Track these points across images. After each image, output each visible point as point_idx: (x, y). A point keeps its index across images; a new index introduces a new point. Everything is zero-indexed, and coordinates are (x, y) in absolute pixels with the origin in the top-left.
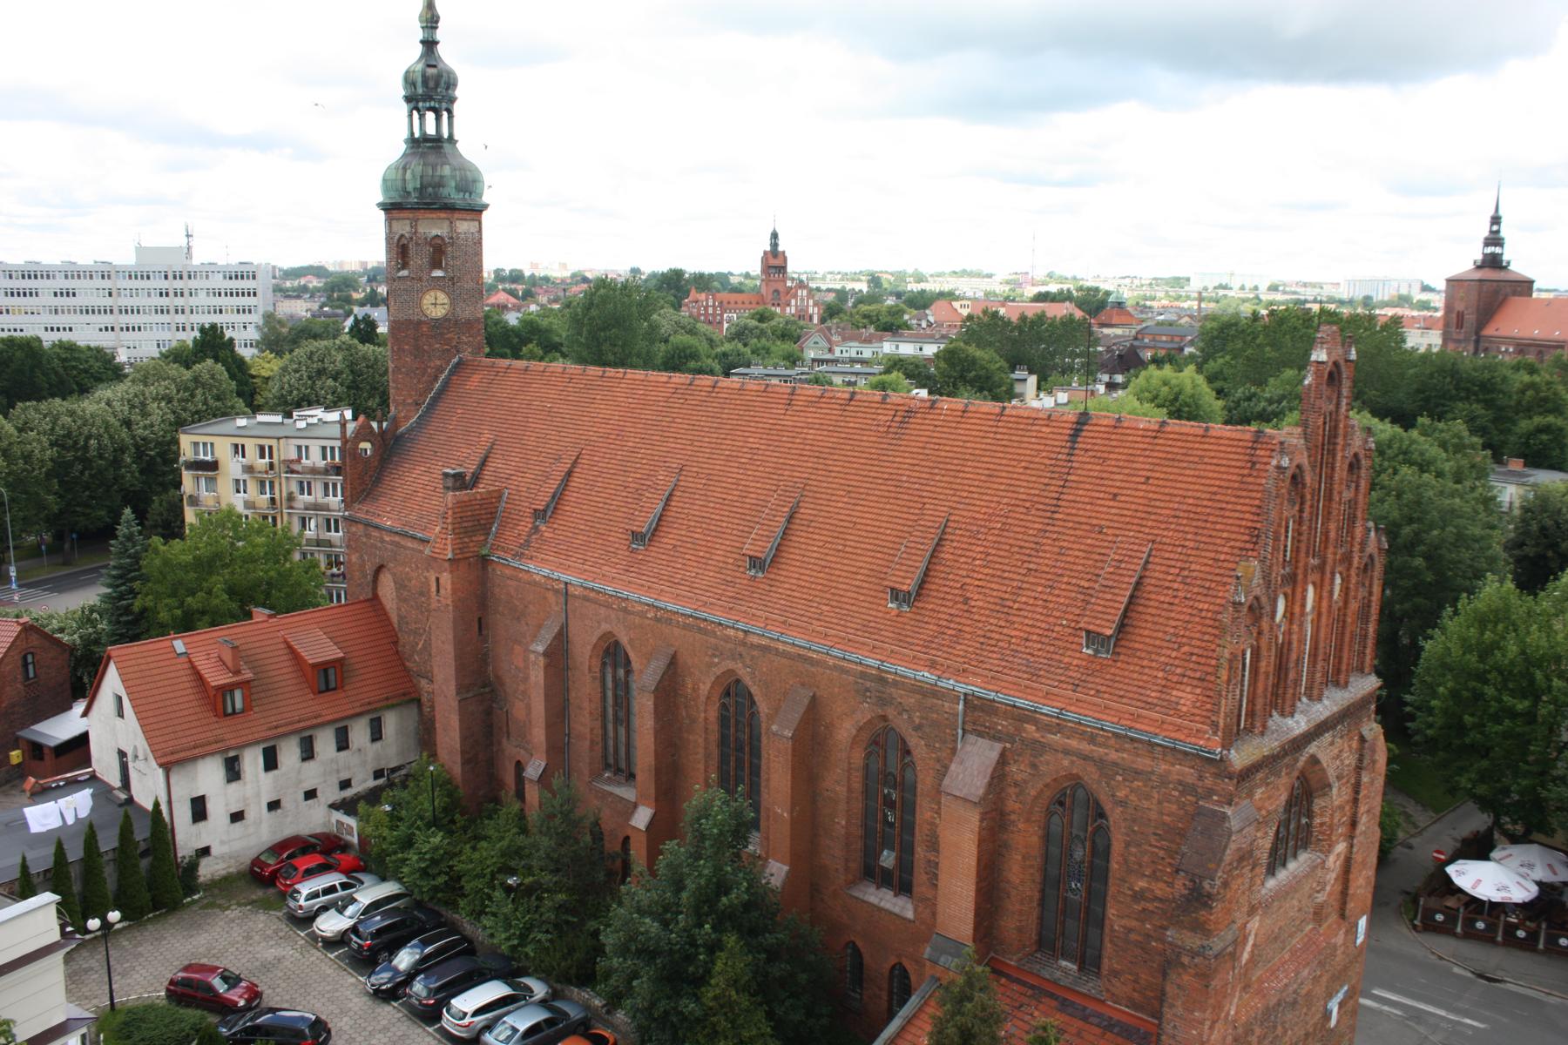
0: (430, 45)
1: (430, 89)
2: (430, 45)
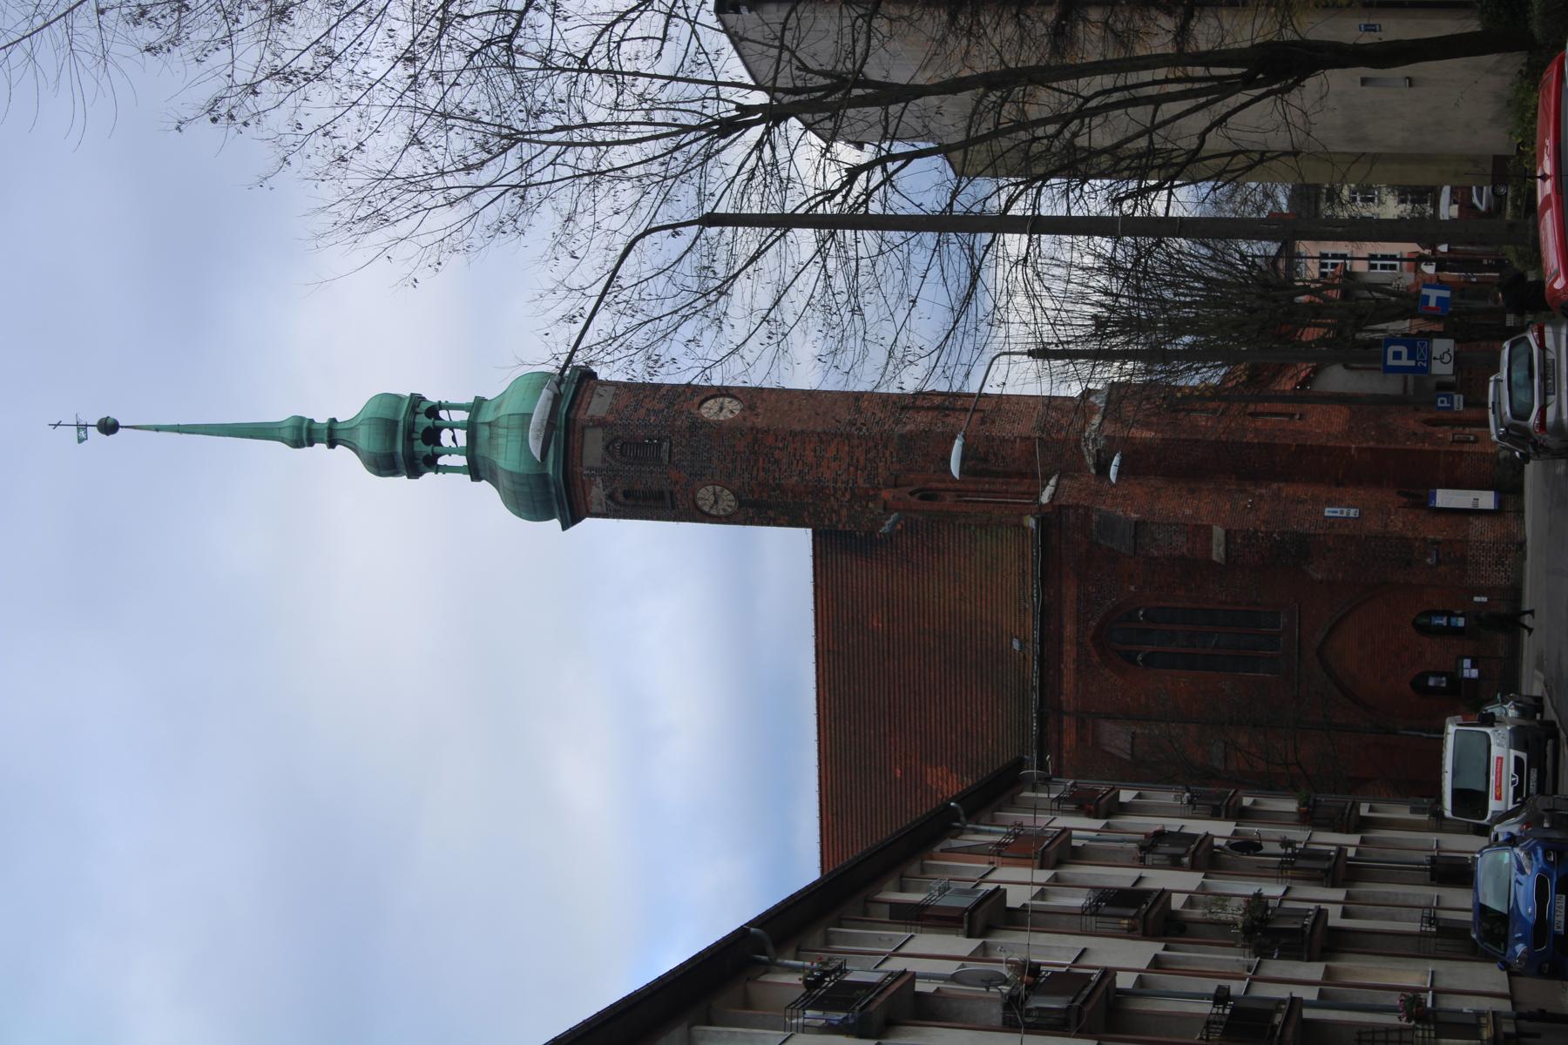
0: (333, 435)
1: (405, 440)
2: (333, 435)
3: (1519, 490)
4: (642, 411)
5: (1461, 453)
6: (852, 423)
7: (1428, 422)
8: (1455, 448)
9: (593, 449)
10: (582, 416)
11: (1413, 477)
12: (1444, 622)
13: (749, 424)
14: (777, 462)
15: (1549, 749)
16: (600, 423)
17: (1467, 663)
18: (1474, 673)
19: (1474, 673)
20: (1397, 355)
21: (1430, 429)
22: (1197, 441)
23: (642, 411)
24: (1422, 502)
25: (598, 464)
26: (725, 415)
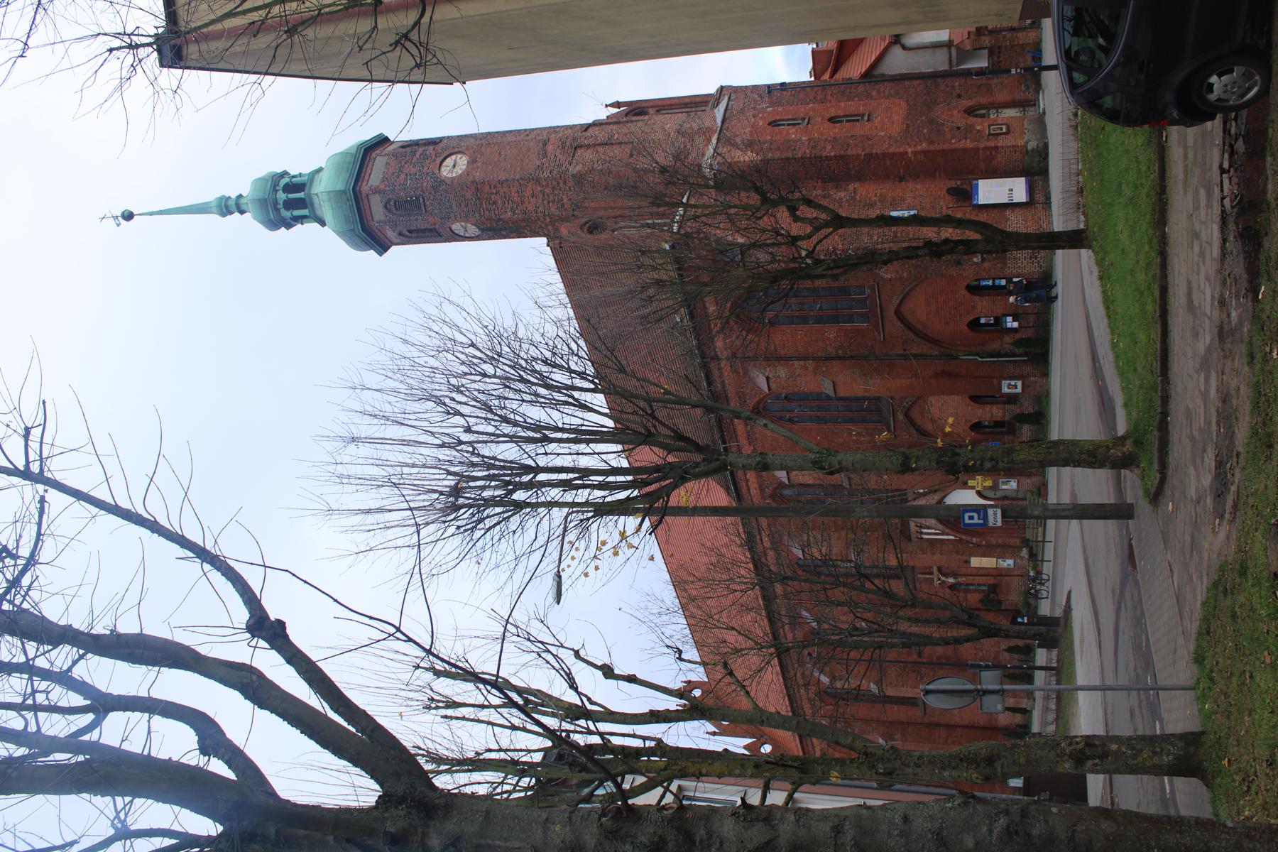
1: (227, 207)
3: (1044, 172)
4: (403, 176)
5: (996, 148)
6: (540, 168)
7: (970, 111)
8: (991, 144)
9: (377, 210)
10: (365, 188)
11: (962, 170)
12: (990, 283)
13: (470, 179)
14: (494, 203)
15: (327, 10)
16: (376, 191)
17: (1009, 319)
18: (1016, 325)
19: (1016, 325)
20: (971, 518)
21: (971, 120)
22: (787, 159)
23: (403, 176)
24: (965, 195)
25: (383, 218)
26: (459, 170)
